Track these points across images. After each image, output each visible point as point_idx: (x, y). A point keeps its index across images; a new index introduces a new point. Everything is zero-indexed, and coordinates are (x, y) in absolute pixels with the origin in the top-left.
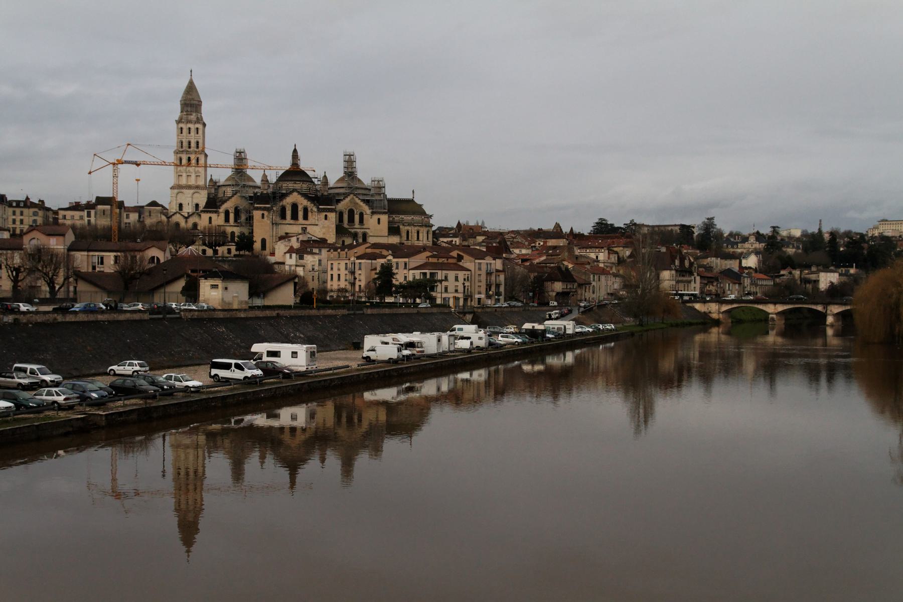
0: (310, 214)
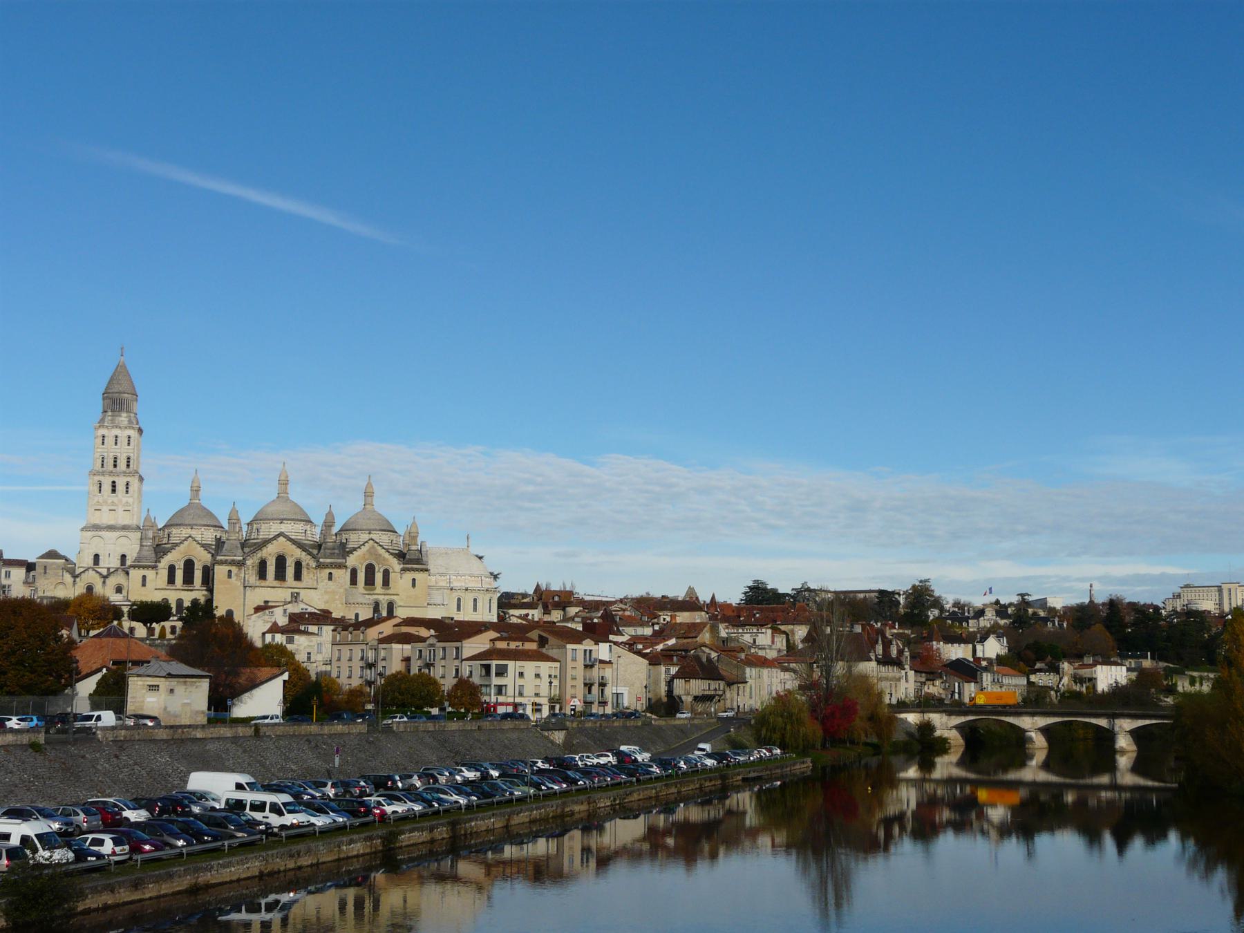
0: (304, 571)
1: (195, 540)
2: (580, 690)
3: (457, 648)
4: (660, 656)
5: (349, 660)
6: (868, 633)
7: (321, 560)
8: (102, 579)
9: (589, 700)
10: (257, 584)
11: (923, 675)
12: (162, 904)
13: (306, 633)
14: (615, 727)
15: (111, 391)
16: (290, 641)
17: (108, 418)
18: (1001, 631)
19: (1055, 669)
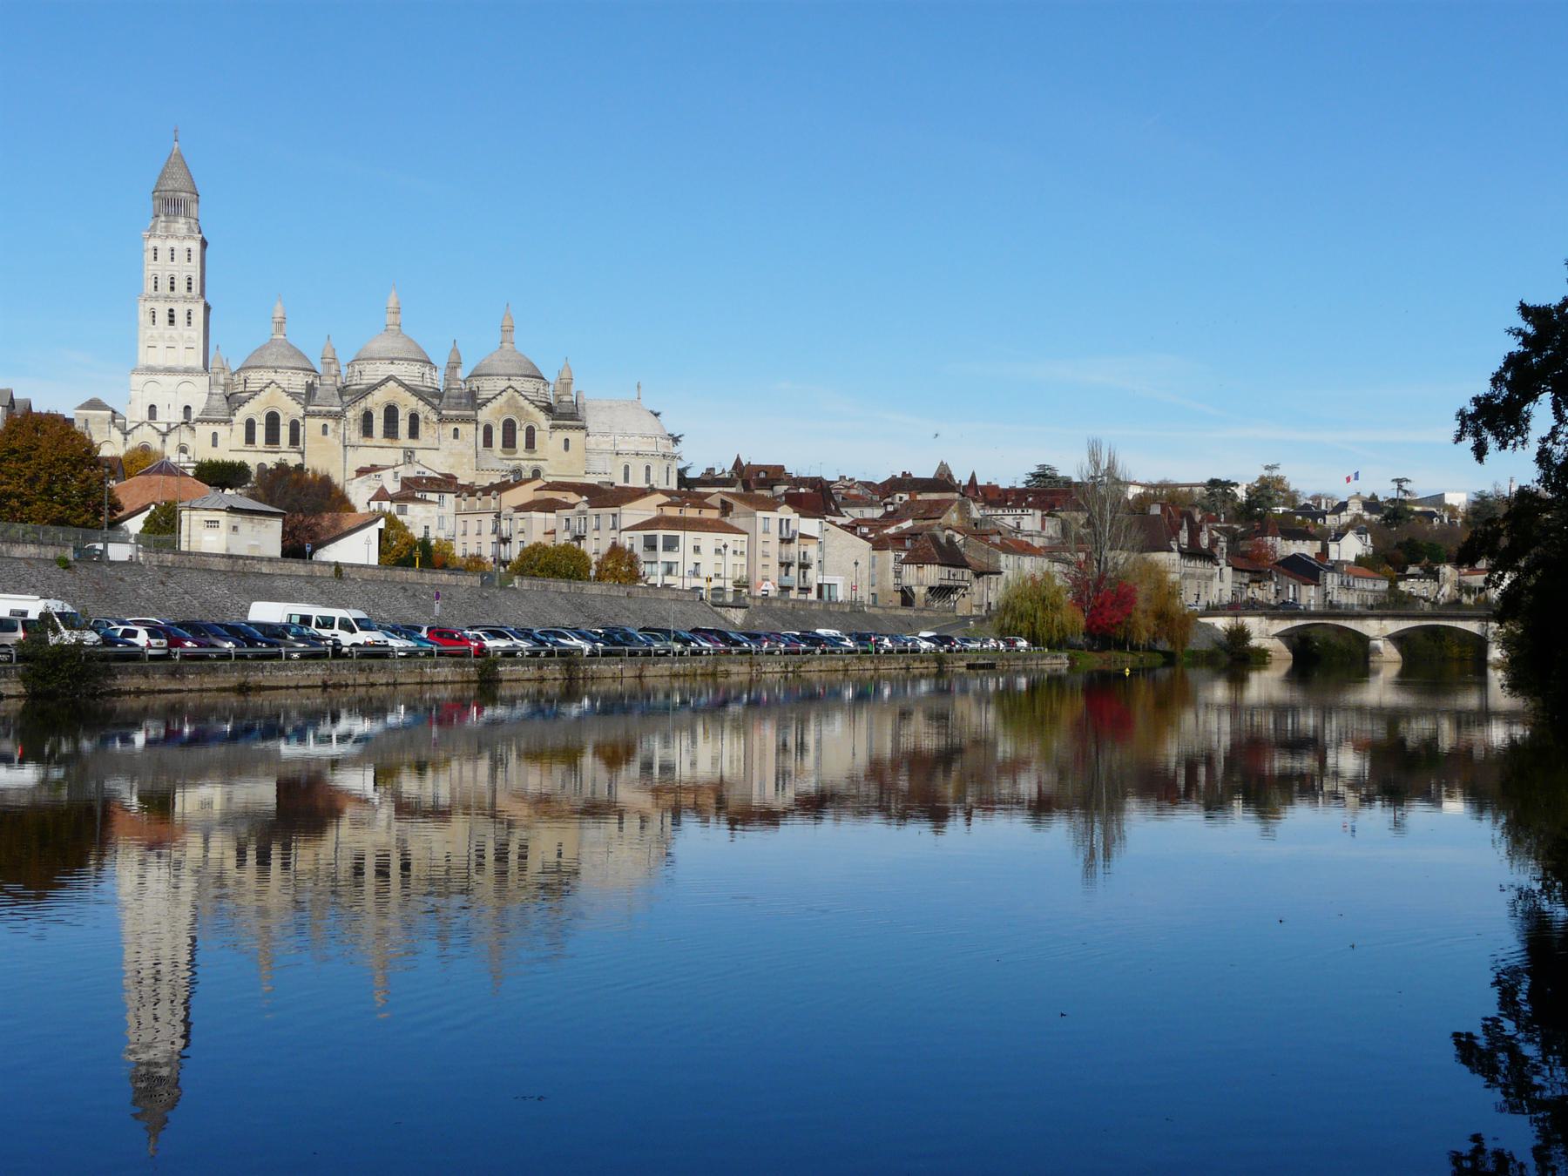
0: (422, 426)
1: (279, 387)
2: (774, 571)
3: (614, 515)
4: (888, 539)
5: (477, 534)
6: (1170, 517)
7: (444, 412)
8: (161, 437)
9: (785, 584)
10: (361, 444)
11: (1246, 574)
12: (205, 701)
13: (423, 501)
14: (813, 610)
15: (163, 188)
16: (403, 511)
17: (161, 225)
18: (1364, 526)
19: (1435, 576)
